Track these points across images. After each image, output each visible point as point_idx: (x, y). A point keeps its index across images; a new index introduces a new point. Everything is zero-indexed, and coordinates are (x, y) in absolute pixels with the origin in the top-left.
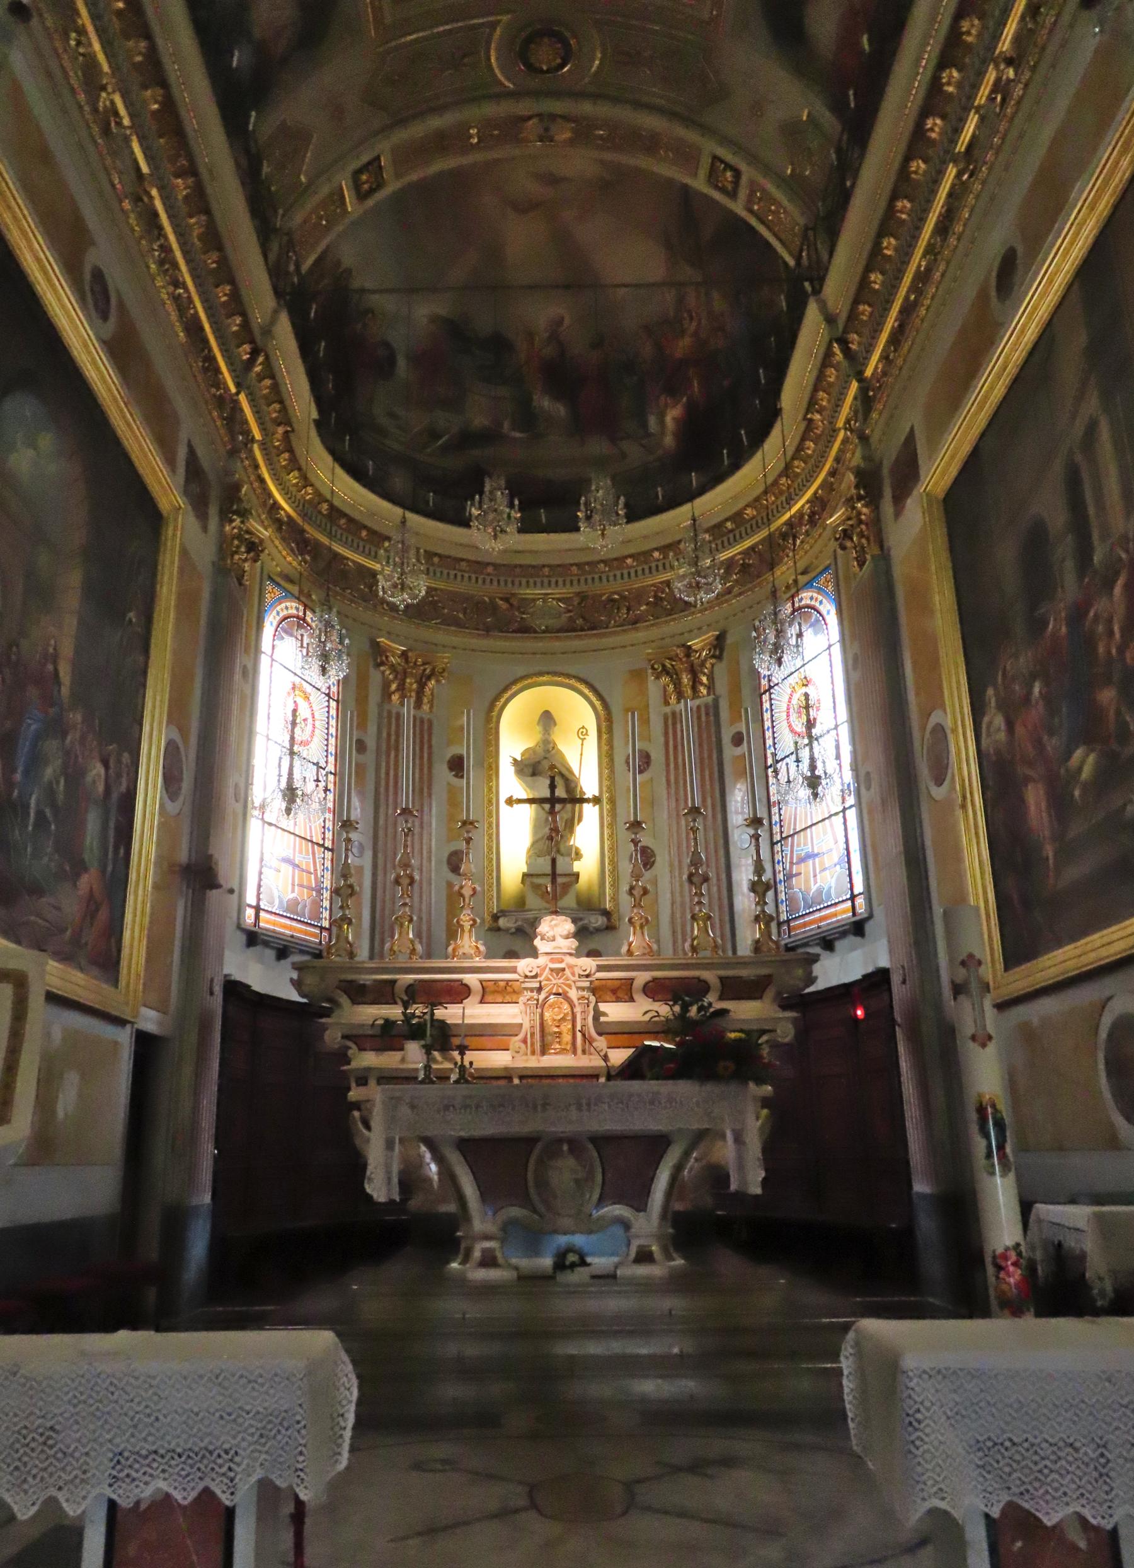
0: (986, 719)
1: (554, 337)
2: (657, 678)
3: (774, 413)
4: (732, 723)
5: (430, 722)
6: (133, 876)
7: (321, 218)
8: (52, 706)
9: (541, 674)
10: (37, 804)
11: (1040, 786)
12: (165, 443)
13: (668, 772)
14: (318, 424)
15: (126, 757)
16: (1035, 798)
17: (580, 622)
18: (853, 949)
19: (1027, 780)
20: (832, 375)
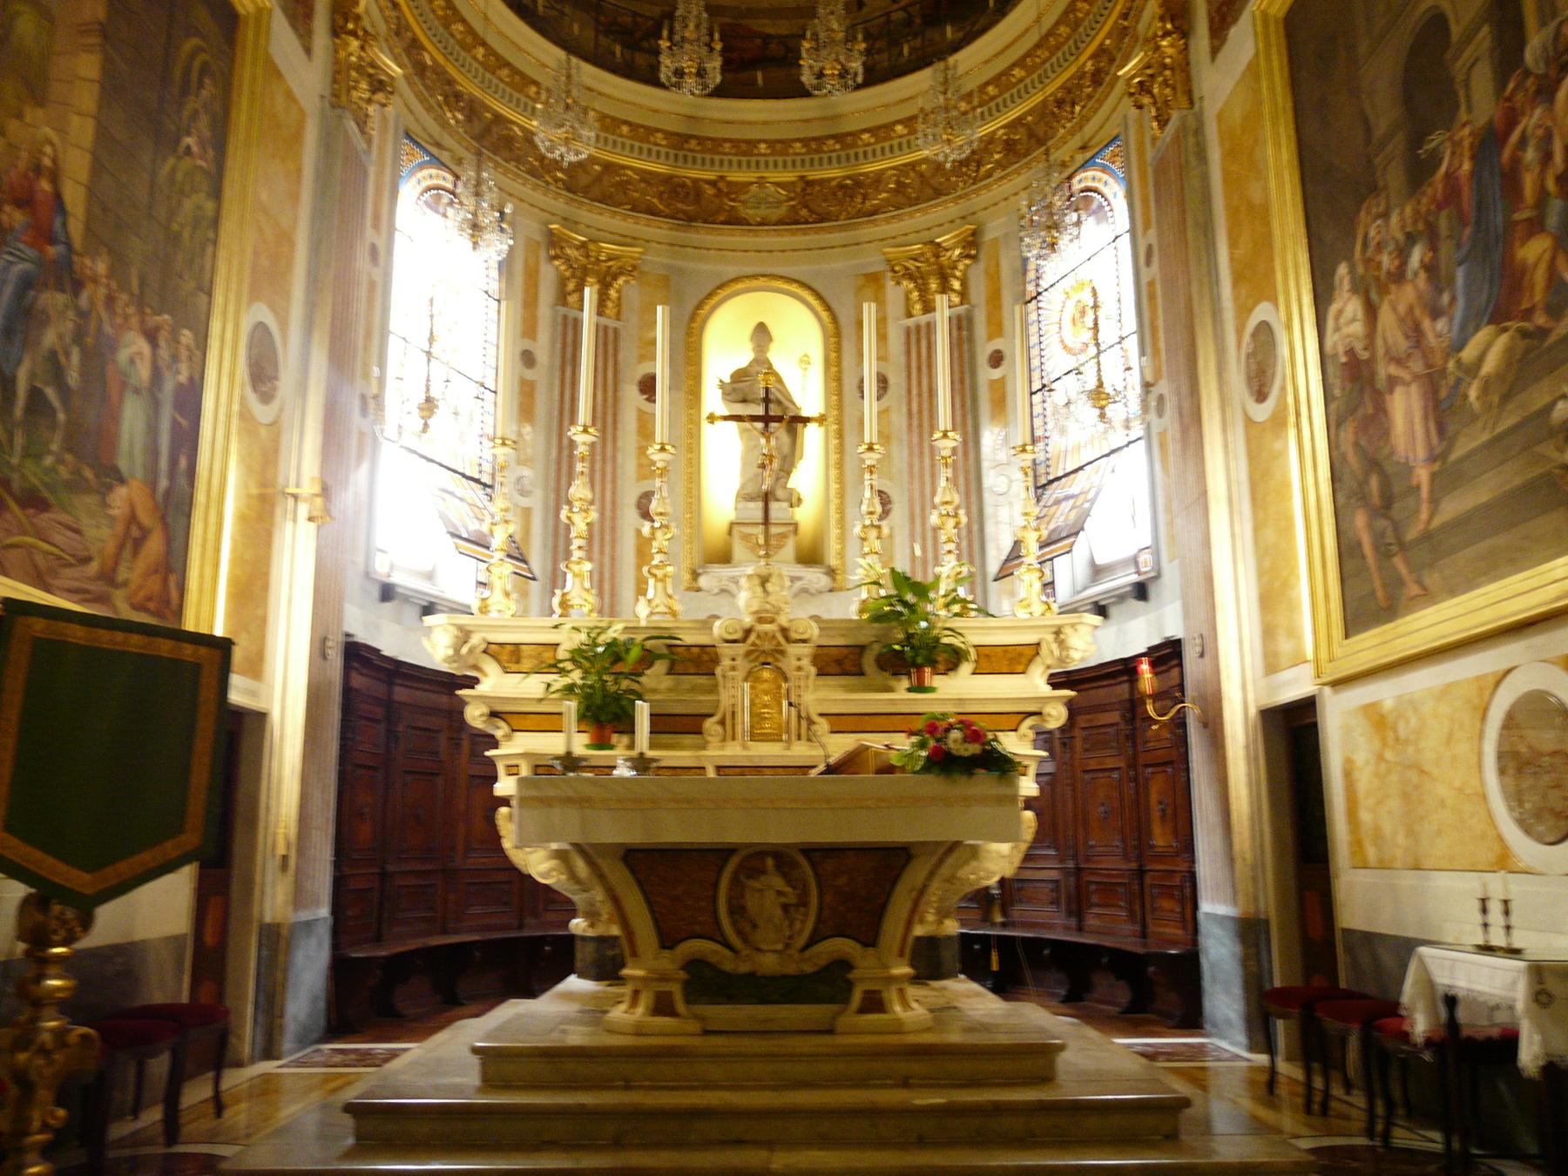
0: (1333, 309)
2: (898, 283)
4: (990, 338)
8: (52, 241)
9: (755, 276)
10: (32, 376)
11: (1414, 388)
13: (909, 403)
16: (1405, 410)
17: (804, 212)
18: (1135, 616)
19: (1393, 382)
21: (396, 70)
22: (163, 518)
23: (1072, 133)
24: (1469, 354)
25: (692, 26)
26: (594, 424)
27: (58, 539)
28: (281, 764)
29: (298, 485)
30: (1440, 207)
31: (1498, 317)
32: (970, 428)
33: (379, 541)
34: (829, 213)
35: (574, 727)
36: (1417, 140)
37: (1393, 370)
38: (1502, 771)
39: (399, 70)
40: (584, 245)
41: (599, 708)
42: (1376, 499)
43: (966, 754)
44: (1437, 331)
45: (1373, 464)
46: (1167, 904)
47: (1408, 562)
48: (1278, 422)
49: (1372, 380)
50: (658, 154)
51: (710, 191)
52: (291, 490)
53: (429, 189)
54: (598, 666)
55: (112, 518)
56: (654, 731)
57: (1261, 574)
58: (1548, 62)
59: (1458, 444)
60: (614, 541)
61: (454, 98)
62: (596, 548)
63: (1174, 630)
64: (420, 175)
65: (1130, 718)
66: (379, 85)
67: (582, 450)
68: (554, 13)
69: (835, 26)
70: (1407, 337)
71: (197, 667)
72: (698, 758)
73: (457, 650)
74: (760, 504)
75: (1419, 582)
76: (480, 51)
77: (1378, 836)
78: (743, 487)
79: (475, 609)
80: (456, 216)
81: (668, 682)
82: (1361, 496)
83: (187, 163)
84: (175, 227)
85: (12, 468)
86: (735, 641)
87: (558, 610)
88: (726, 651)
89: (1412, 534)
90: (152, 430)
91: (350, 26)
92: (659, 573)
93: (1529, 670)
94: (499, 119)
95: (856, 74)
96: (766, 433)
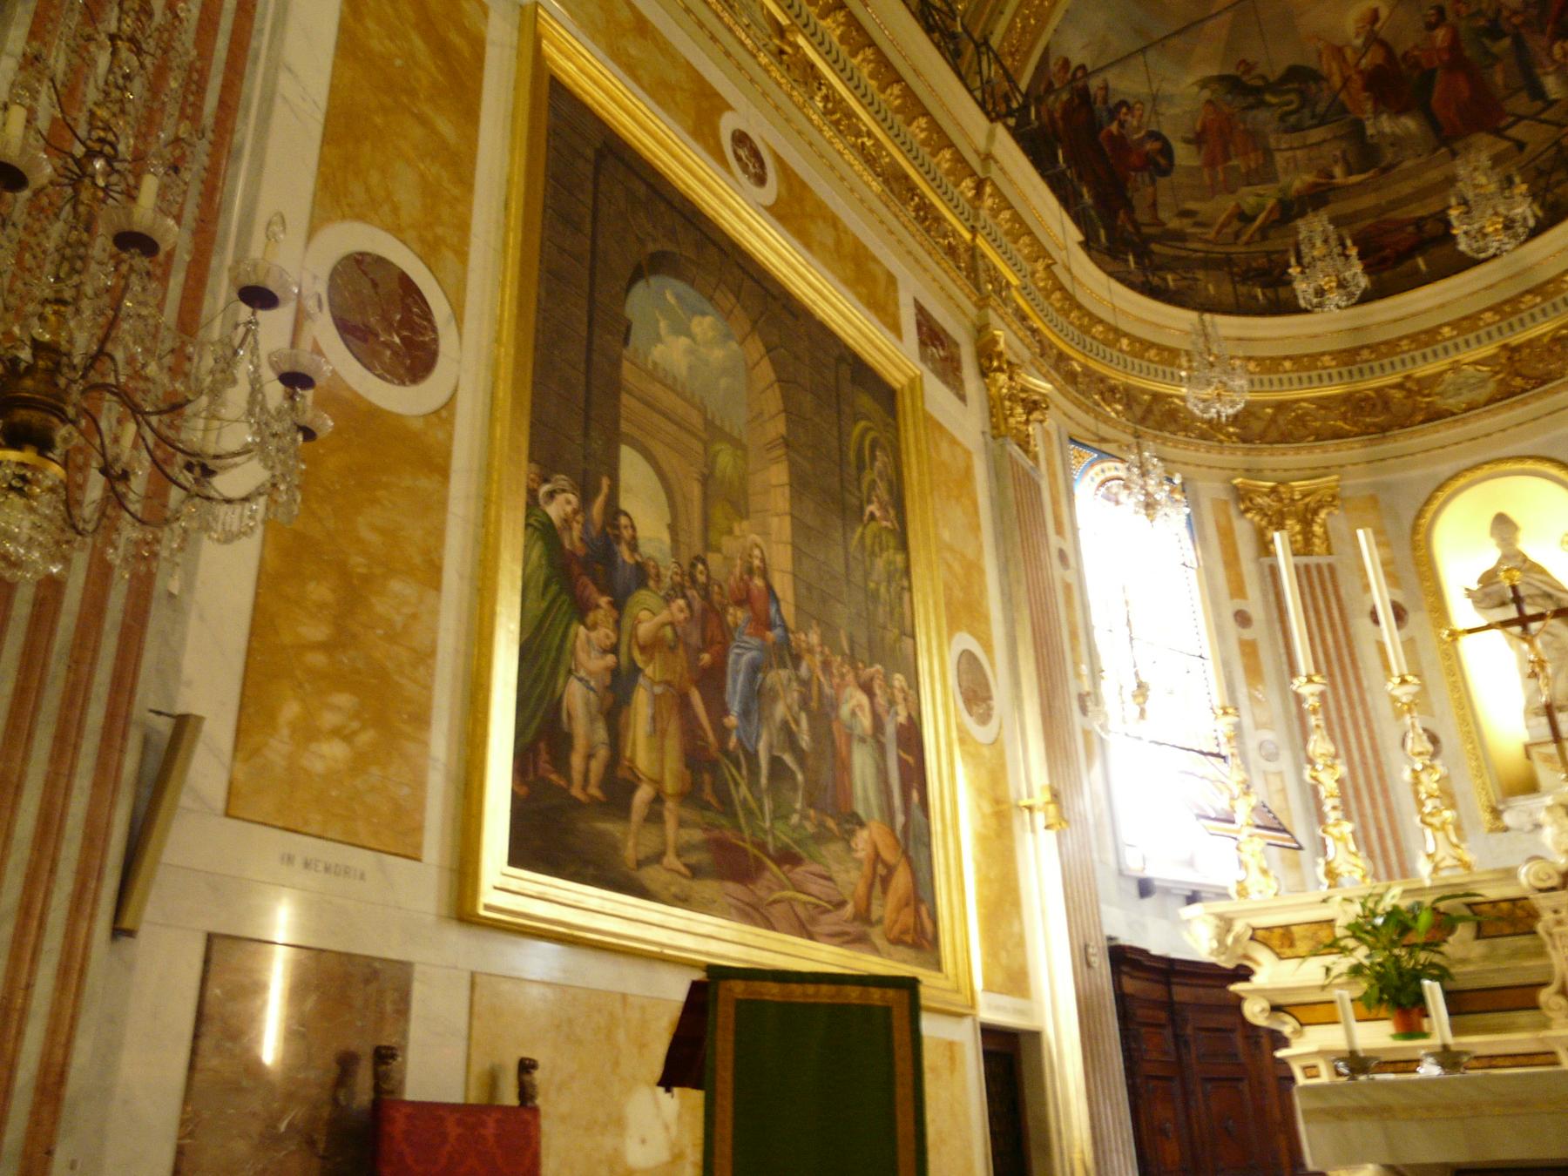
1: (1373, 39)
5: (1331, 568)
6: (936, 826)
7: (1028, 18)
8: (770, 626)
9: (1477, 466)
10: (771, 747)
12: (881, 305)
14: (1086, 245)
15: (899, 680)
17: (1518, 382)
21: (1044, 386)
22: (905, 853)
25: (1319, 243)
26: (1318, 671)
27: (813, 888)
28: (1064, 1080)
29: (1030, 796)
33: (1125, 835)
34: (1549, 373)
35: (1351, 1017)
39: (1049, 386)
40: (1273, 490)
41: (1398, 990)
50: (1330, 376)
51: (1398, 395)
52: (1025, 802)
53: (1103, 483)
54: (1384, 940)
55: (859, 862)
56: (1452, 1013)
60: (1385, 792)
61: (1111, 393)
62: (1353, 805)
64: (1092, 472)
66: (1033, 406)
67: (1311, 702)
68: (1185, 283)
69: (1482, 180)
71: (887, 1011)
72: (1542, 1040)
73: (1221, 942)
74: (1544, 720)
76: (1125, 342)
78: (1529, 702)
79: (1232, 891)
80: (1131, 502)
81: (1478, 948)
83: (873, 525)
84: (872, 585)
85: (765, 832)
86: (1552, 889)
87: (1326, 882)
88: (1543, 902)
90: (882, 773)
91: (995, 364)
92: (1436, 821)
94: (1156, 397)
95: (1525, 219)
96: (1526, 636)
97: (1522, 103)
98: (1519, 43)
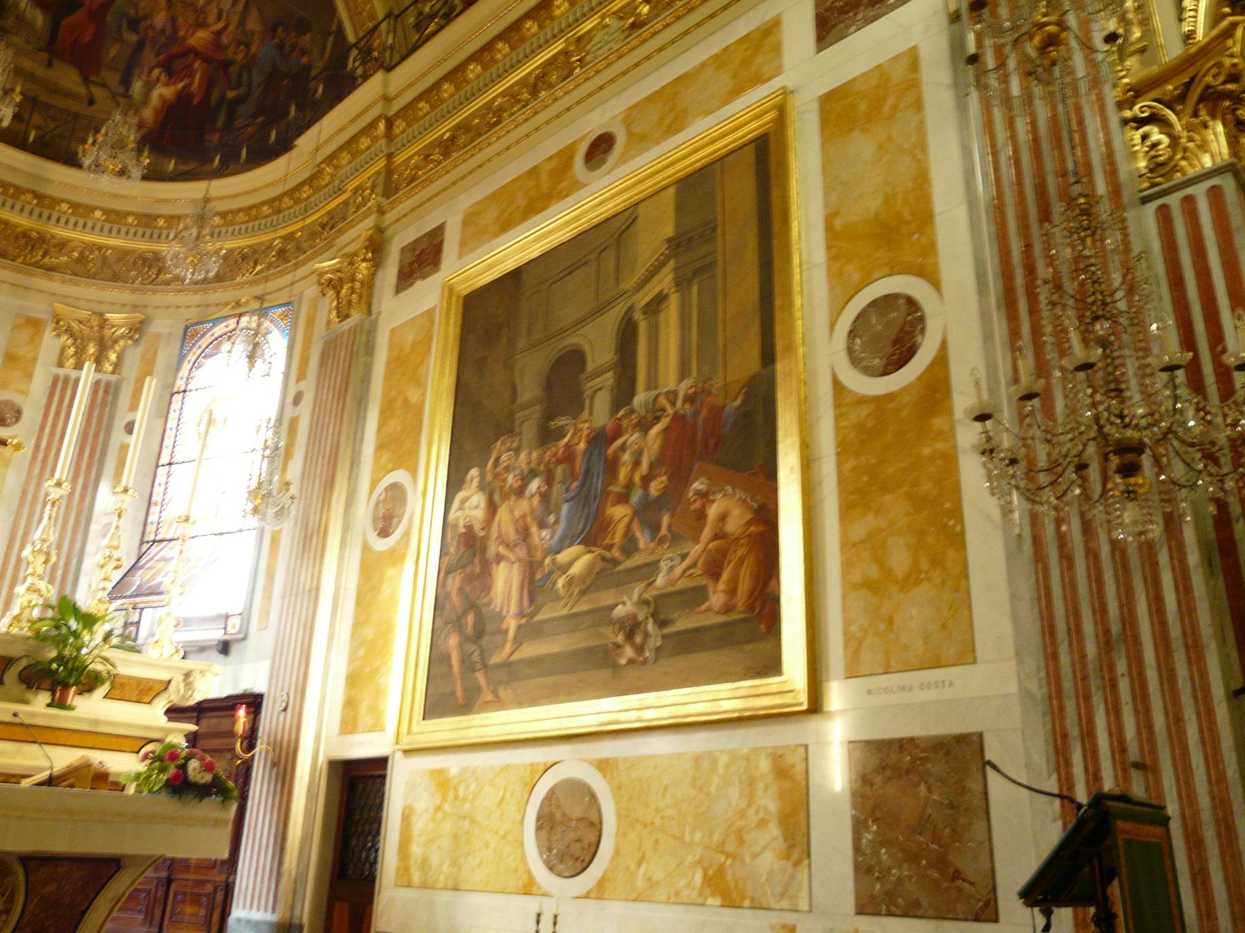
2: (58, 335)
3: (284, 146)
11: (516, 566)
16: (506, 581)
19: (499, 558)
20: (364, 142)
23: (252, 283)
24: (563, 557)
30: (559, 462)
31: (589, 542)
32: (93, 476)
36: (549, 415)
37: (501, 549)
38: (539, 828)
42: (469, 629)
43: (203, 781)
44: (542, 537)
45: (472, 606)
46: (189, 909)
47: (487, 677)
48: (396, 556)
49: (484, 550)
57: (352, 658)
58: (647, 411)
59: (543, 610)
63: (259, 687)
65: (218, 749)
70: (517, 532)
75: (495, 692)
77: (425, 864)
82: (458, 624)
89: (495, 659)
93: (573, 765)
97: (113, 79)
98: (140, 46)
